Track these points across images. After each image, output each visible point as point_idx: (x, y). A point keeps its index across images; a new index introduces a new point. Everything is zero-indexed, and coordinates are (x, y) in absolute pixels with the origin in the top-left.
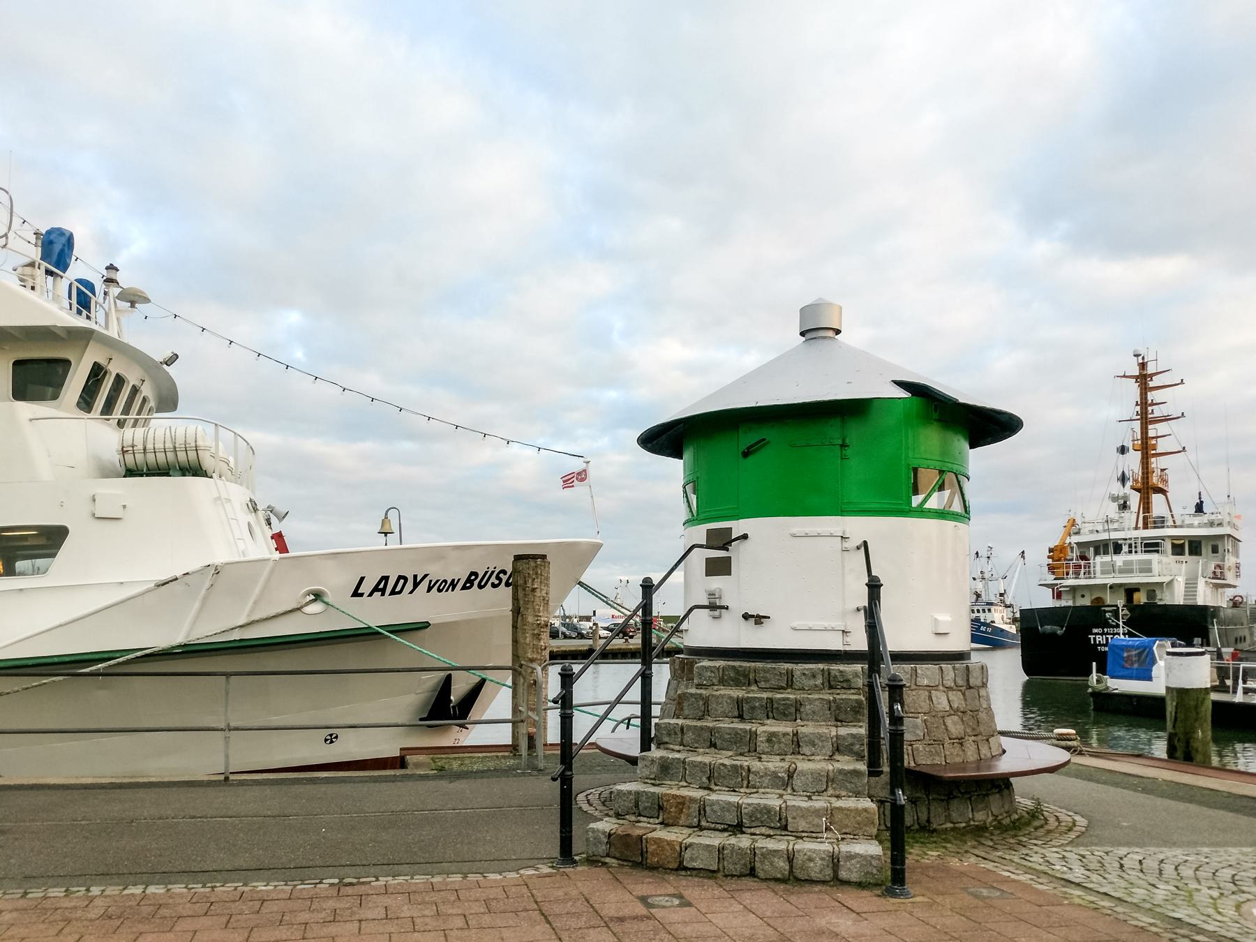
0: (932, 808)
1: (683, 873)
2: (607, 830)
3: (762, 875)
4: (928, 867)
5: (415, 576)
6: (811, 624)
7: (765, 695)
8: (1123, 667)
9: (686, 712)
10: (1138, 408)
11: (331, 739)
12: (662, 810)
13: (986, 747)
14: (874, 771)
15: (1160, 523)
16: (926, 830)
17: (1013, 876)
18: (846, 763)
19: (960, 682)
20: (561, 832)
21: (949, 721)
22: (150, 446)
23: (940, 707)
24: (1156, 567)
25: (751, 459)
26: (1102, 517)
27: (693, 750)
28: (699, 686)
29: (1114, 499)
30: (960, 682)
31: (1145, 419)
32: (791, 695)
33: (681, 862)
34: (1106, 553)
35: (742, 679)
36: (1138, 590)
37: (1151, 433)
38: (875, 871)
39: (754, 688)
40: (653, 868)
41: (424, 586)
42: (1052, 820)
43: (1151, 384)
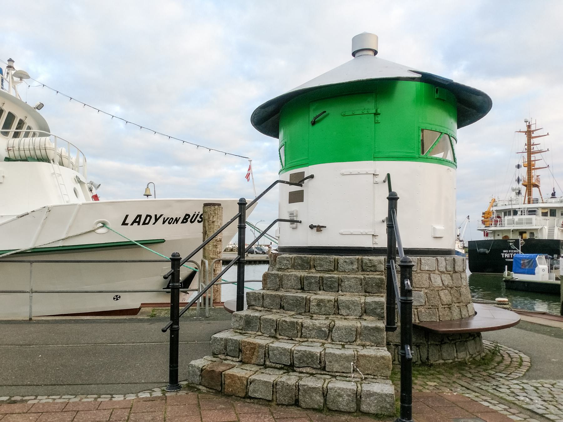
0: (430, 350)
1: (248, 400)
2: (201, 366)
3: (303, 405)
4: (428, 397)
5: (156, 216)
6: (352, 231)
7: (318, 275)
8: (520, 268)
9: (269, 286)
10: (526, 147)
11: (117, 298)
12: (242, 353)
13: (466, 310)
14: (390, 328)
15: (537, 201)
16: (426, 364)
17: (491, 407)
18: (371, 322)
19: (449, 268)
20: (170, 367)
21: (442, 294)
22: (22, 147)
23: (436, 284)
24: (534, 221)
25: (317, 126)
26: (508, 198)
27: (270, 311)
28: (280, 269)
29: (513, 190)
30: (449, 268)
31: (530, 152)
32: (335, 275)
33: (247, 393)
34: (510, 215)
35: (307, 265)
36: (525, 232)
37: (532, 159)
38: (388, 406)
39: (313, 270)
40: (228, 396)
41: (161, 220)
42: (506, 356)
43: (533, 135)
